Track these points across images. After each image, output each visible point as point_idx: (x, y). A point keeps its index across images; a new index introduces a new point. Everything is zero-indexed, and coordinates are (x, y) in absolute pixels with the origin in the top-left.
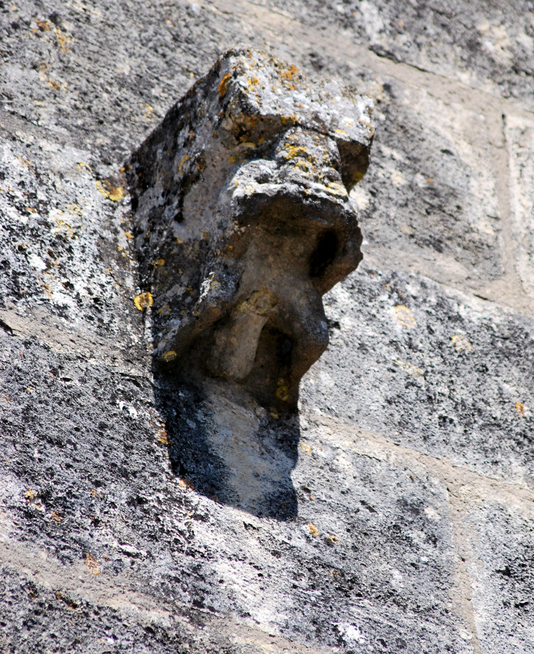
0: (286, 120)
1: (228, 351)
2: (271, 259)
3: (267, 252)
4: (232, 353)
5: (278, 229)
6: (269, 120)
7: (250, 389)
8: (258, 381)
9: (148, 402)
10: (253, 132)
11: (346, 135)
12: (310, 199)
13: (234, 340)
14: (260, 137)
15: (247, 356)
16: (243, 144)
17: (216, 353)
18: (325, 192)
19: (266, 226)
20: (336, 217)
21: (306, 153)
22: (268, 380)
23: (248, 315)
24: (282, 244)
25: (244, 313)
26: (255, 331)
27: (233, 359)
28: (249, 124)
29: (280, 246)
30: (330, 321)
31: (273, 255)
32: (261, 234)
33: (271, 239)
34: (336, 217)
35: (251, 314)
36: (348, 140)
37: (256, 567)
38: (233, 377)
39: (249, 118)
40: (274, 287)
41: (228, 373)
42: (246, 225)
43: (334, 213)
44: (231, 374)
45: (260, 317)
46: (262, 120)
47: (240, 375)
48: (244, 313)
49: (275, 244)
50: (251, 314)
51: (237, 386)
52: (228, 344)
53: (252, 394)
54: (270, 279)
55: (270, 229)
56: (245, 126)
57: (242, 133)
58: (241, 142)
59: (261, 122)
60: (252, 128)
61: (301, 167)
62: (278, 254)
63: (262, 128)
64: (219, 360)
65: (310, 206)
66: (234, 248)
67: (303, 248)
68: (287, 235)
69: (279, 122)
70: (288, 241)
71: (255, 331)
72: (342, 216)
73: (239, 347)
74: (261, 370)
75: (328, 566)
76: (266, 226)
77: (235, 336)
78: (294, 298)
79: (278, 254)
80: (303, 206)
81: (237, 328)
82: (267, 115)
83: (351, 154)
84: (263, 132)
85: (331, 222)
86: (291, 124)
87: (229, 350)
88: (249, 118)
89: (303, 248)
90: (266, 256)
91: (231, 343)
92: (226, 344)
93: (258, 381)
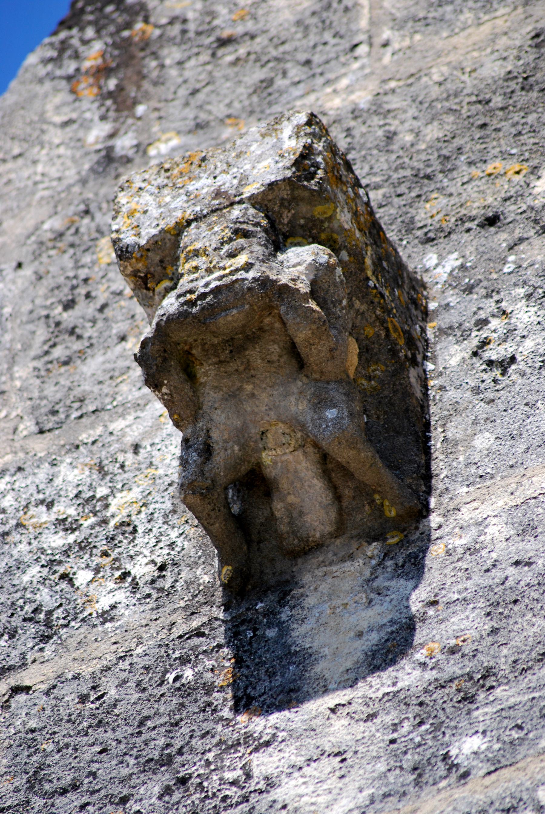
0: (174, 228)
1: (295, 514)
2: (249, 388)
3: (238, 384)
4: (301, 514)
5: (231, 351)
6: (155, 243)
7: (354, 532)
8: (359, 517)
9: (214, 647)
10: (152, 269)
11: (258, 185)
12: (199, 302)
13: (291, 499)
14: (165, 268)
15: (321, 503)
16: (157, 289)
17: (283, 528)
18: (215, 280)
19: (215, 360)
20: (243, 295)
21: (195, 250)
22: (367, 508)
23: (282, 462)
24: (248, 361)
25: (275, 463)
26: (307, 469)
27: (308, 519)
28: (140, 266)
29: (248, 366)
30: (503, 361)
31: (248, 382)
32: (213, 373)
33: (232, 366)
34: (243, 295)
35: (284, 458)
36: (263, 188)
37: (336, 755)
38: (322, 536)
39: (134, 260)
40: (272, 413)
41: (314, 536)
42: (162, 385)
43: (236, 294)
44: (318, 535)
45: (296, 453)
46: (148, 250)
47: (329, 529)
48: (275, 463)
49: (241, 368)
50: (284, 458)
51: (338, 542)
52: (289, 508)
53: (359, 537)
54: (264, 409)
55: (222, 358)
56: (139, 271)
57: (145, 280)
58: (154, 290)
59: (150, 254)
60: (147, 267)
61: (190, 272)
62: (252, 376)
63: (158, 258)
64: (293, 532)
65: (203, 309)
66: (179, 415)
67: (276, 346)
68: (246, 349)
69: (169, 236)
70: (254, 355)
71: (307, 469)
72: (249, 289)
73: (303, 501)
74: (354, 503)
75: (451, 681)
76: (215, 360)
77: (289, 494)
78: (293, 409)
79: (252, 376)
80: (195, 316)
81: (284, 484)
82: (148, 242)
83: (283, 199)
84: (161, 261)
85: (243, 305)
86: (182, 226)
87: (295, 514)
88: (134, 260)
89: (276, 346)
90: (240, 389)
91: (291, 505)
92: (288, 510)
93: (359, 517)
